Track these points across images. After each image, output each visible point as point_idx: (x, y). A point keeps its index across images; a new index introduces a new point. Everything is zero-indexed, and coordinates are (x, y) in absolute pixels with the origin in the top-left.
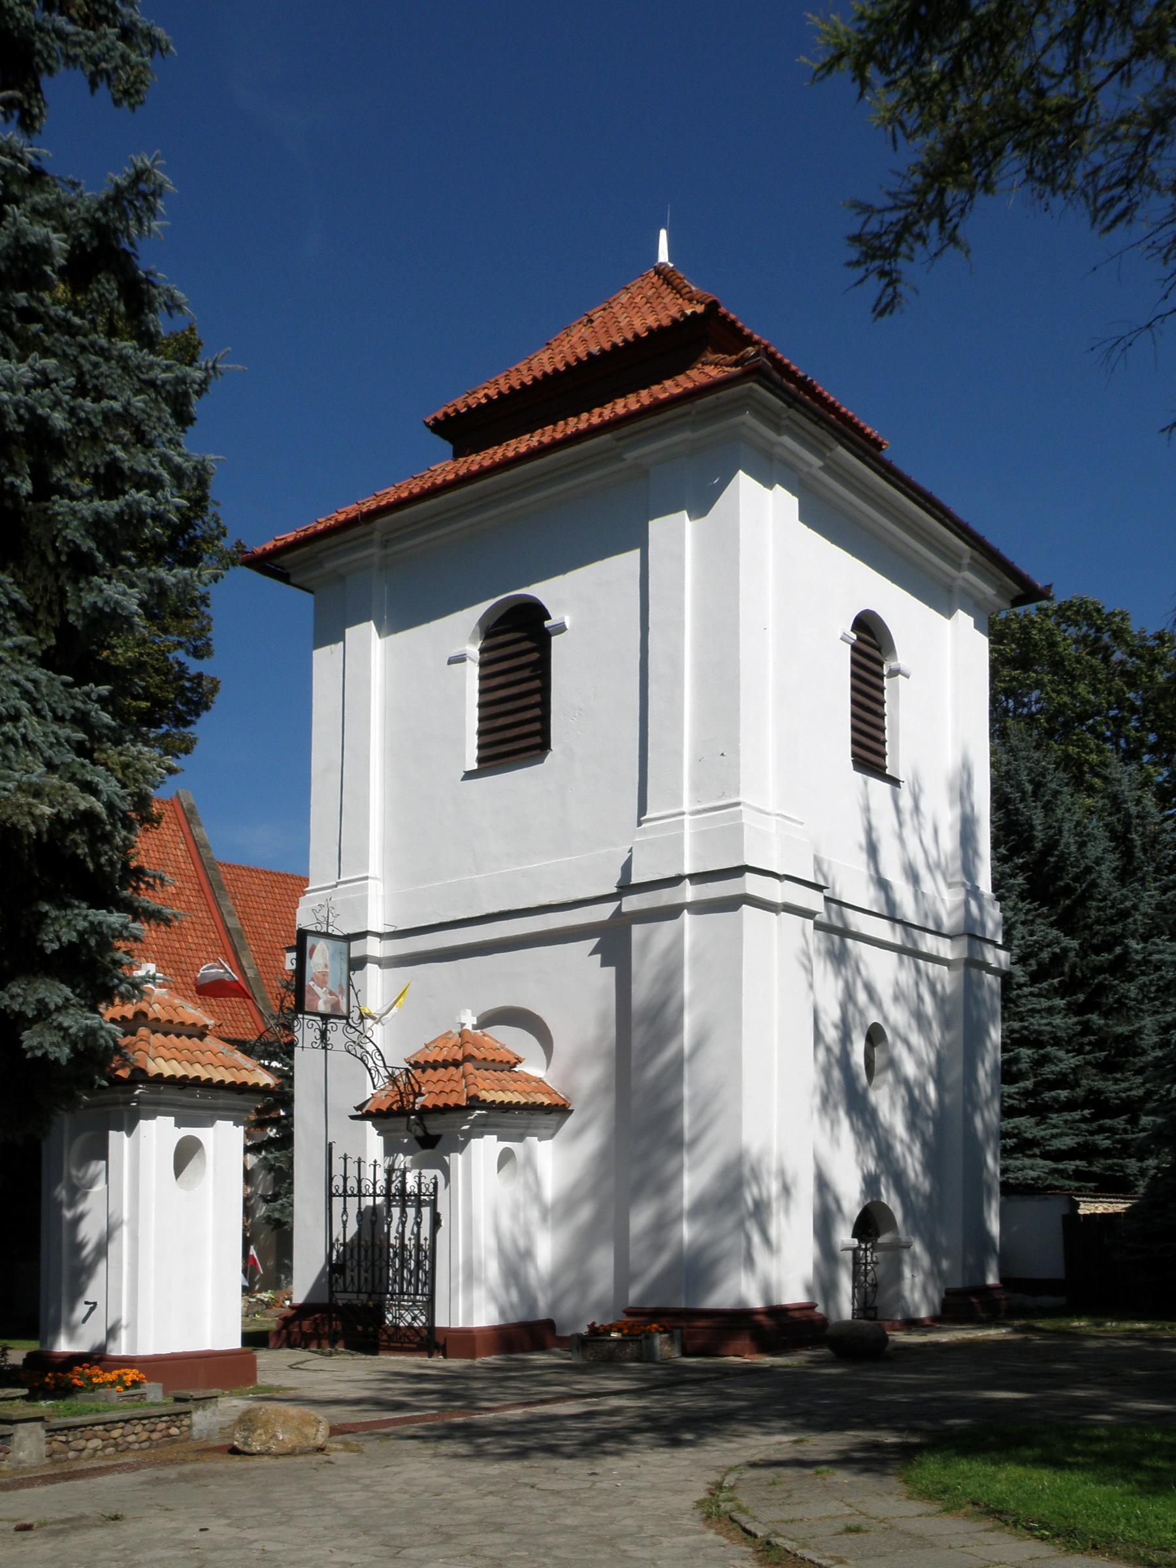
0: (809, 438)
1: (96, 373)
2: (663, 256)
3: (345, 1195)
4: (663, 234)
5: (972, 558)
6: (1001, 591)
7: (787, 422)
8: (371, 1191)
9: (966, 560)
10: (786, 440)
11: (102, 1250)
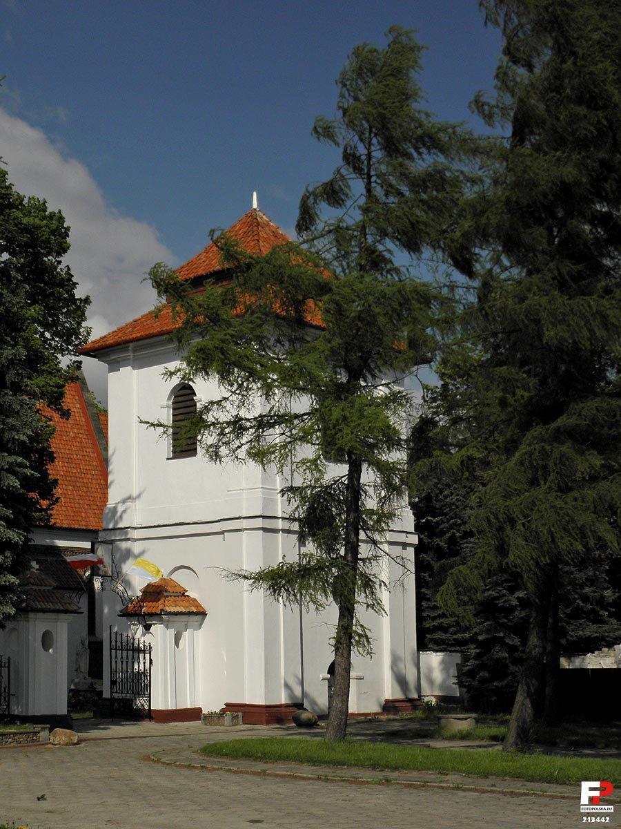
2: (255, 205)
3: (116, 649)
4: (255, 193)
11: (409, 253)
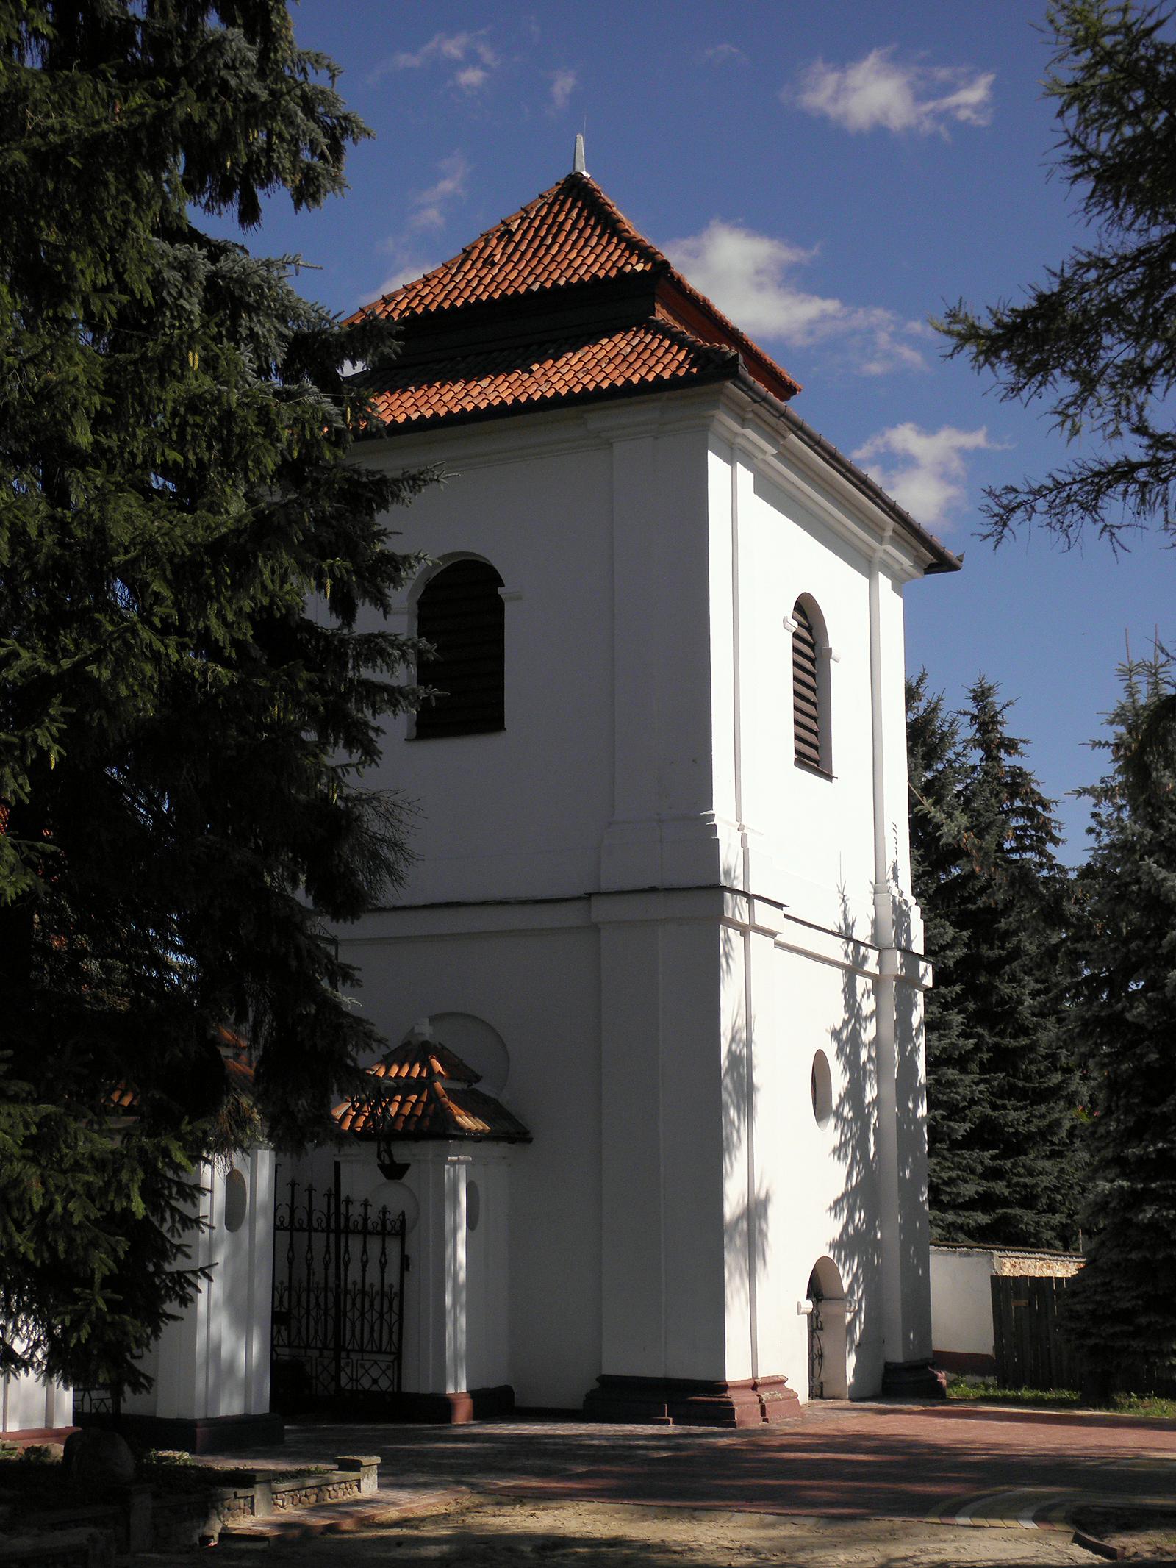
0: (768, 429)
1: (1091, 1063)
4: (581, 139)
5: (894, 531)
6: (917, 560)
7: (750, 416)
8: (324, 1225)
9: (889, 533)
10: (749, 432)
